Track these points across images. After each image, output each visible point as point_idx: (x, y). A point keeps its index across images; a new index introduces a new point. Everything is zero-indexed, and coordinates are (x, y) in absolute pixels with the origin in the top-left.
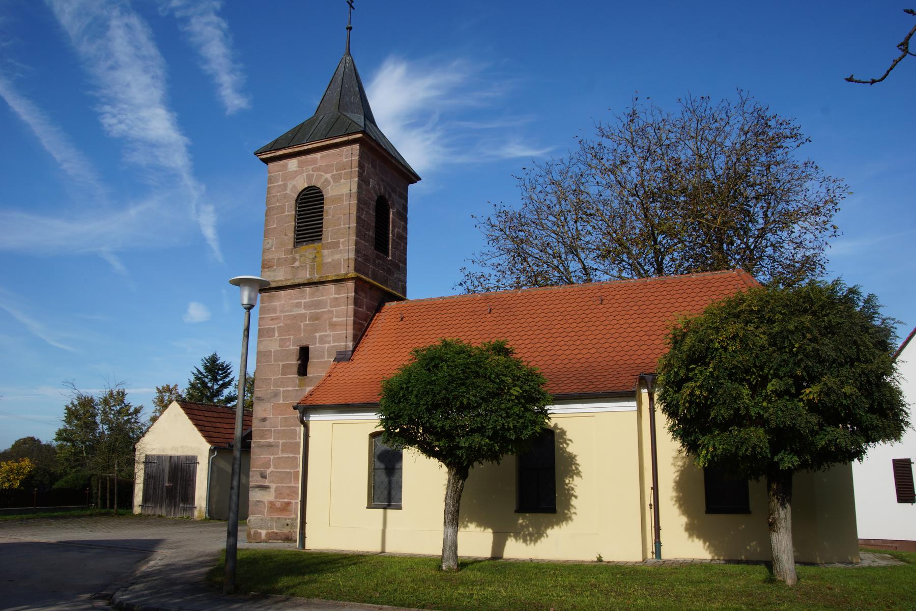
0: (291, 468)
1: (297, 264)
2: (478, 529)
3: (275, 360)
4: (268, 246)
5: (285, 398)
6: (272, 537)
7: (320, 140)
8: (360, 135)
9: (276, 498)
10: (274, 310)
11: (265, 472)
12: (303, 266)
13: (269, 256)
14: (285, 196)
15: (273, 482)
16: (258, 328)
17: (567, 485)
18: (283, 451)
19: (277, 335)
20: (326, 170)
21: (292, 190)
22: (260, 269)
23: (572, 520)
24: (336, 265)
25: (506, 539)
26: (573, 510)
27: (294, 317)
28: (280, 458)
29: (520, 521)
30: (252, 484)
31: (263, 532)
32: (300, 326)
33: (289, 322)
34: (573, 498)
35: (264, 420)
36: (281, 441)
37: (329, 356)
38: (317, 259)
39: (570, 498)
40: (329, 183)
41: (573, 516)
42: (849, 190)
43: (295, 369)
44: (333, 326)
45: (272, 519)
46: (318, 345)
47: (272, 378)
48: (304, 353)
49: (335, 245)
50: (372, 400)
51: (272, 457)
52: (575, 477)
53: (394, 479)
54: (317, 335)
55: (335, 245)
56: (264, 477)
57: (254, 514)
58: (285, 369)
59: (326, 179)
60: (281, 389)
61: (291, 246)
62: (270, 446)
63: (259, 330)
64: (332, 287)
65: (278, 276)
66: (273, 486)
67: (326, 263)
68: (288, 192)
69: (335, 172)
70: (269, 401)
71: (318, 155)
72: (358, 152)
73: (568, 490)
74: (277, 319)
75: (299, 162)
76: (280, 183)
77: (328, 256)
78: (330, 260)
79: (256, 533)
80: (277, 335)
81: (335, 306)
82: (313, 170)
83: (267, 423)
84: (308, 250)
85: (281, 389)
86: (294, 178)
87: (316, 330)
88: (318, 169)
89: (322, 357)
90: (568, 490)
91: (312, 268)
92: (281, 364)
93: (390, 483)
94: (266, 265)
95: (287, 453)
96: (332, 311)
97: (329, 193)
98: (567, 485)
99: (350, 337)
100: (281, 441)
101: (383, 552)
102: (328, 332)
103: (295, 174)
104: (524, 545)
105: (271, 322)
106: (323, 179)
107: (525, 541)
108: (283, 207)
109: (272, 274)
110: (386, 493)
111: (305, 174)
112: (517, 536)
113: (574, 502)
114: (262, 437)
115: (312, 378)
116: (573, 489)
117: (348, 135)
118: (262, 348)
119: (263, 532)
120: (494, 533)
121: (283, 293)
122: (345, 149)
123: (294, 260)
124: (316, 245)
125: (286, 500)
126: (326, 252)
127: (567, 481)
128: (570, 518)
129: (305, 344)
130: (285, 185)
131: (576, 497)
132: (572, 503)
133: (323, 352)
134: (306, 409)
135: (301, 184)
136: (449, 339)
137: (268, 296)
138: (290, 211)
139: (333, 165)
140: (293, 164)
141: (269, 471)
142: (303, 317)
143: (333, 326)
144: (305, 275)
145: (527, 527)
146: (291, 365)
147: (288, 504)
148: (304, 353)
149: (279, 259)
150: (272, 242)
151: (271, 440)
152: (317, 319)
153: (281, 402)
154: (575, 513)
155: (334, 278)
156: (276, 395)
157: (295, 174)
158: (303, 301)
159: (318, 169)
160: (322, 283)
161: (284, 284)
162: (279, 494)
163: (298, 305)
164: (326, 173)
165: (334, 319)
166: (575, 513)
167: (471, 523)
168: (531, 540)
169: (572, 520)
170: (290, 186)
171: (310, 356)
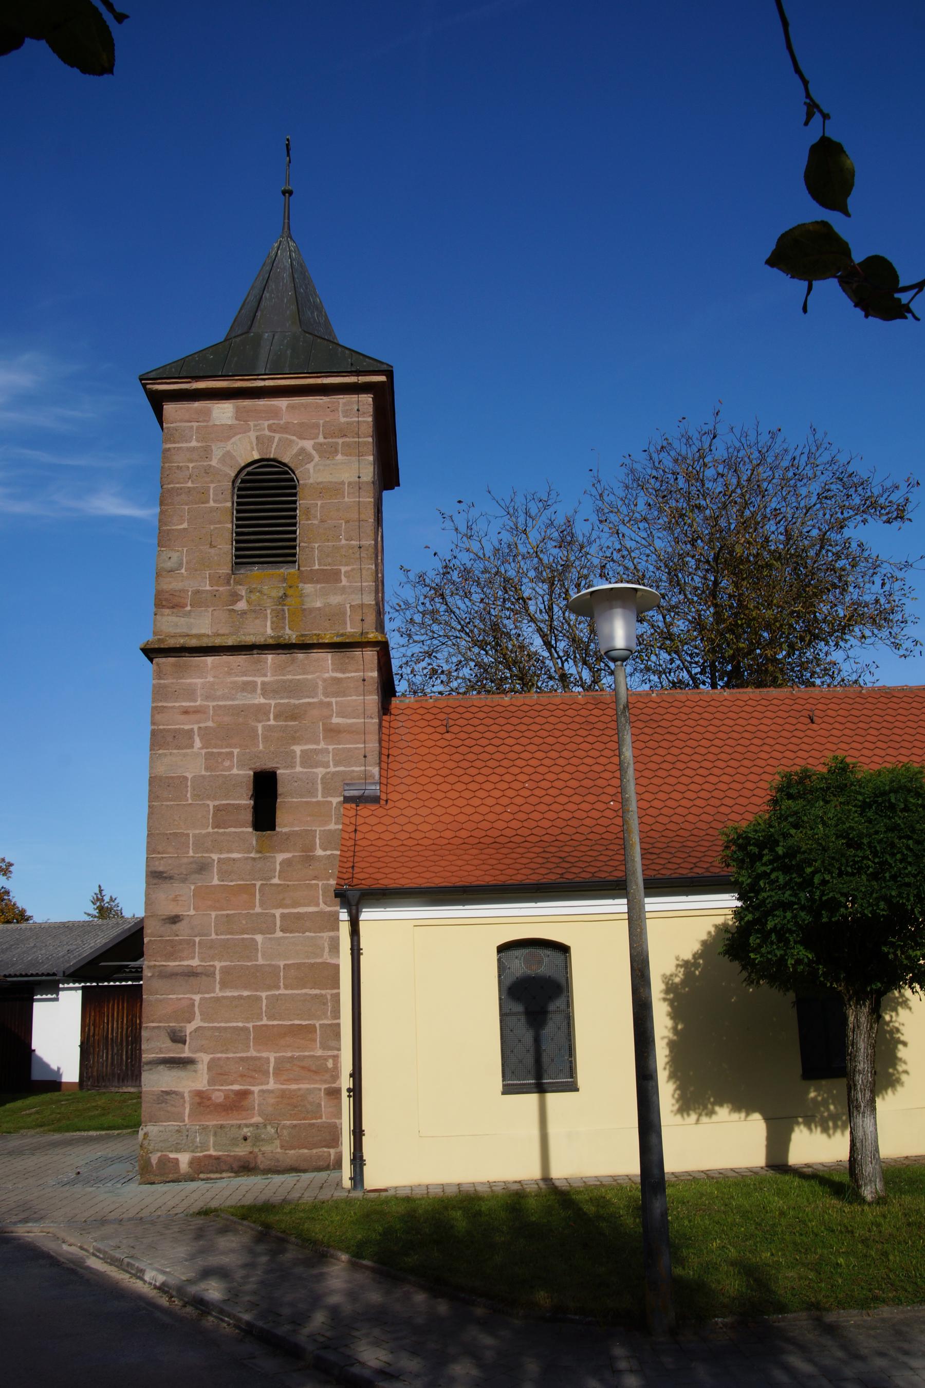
0: (247, 1020)
1: (242, 605)
2: (735, 1116)
3: (196, 796)
4: (169, 565)
5: (223, 875)
6: (205, 1168)
7: (296, 372)
8: (383, 378)
9: (211, 1082)
10: (190, 693)
11: (182, 1030)
12: (257, 611)
13: (171, 584)
14: (207, 471)
15: (202, 1049)
16: (149, 728)
17: (888, 1024)
18: (224, 985)
19: (198, 743)
20: (303, 431)
21: (222, 460)
22: (153, 609)
23: (902, 1084)
24: (336, 615)
25: (791, 1130)
26: (901, 1067)
27: (241, 710)
28: (217, 1000)
29: (812, 1095)
30: (146, 1057)
31: (184, 1159)
32: (255, 730)
33: (227, 719)
34: (900, 1047)
35: (175, 919)
36: (218, 965)
37: (327, 791)
38: (288, 601)
39: (896, 1047)
40: (310, 458)
41: (904, 1077)
42: (913, 595)
43: (248, 816)
44: (332, 732)
45: (205, 1128)
46: (299, 769)
47: (191, 832)
48: (265, 787)
49: (330, 577)
50: (718, 869)
51: (197, 998)
52: (900, 1009)
53: (549, 1030)
54: (298, 749)
55: (332, 577)
56: (178, 1038)
57: (154, 1120)
58: (222, 816)
59: (303, 450)
60: (215, 857)
61: (226, 570)
62: (192, 974)
63: (154, 733)
64: (327, 658)
65: (202, 625)
66: (204, 1059)
67: (311, 610)
68: (214, 463)
69: (321, 439)
70: (184, 880)
71: (282, 403)
72: (370, 409)
73: (891, 1032)
74: (197, 711)
75: (238, 410)
76: (194, 444)
77: (315, 597)
78: (319, 604)
79: (164, 1161)
80: (198, 743)
81: (336, 694)
82: (270, 428)
83: (180, 926)
84: (266, 581)
85: (215, 857)
86: (229, 438)
87: (295, 740)
88: (285, 428)
89: (312, 792)
90: (891, 1032)
91: (279, 616)
92: (211, 804)
93: (537, 1041)
94: (165, 601)
95: (236, 988)
96: (329, 704)
97: (313, 474)
98: (888, 1024)
99: (373, 757)
100: (282, 964)
101: (546, 1179)
102: (322, 745)
103: (228, 432)
104: (824, 1136)
105: (183, 718)
106: (295, 450)
107: (825, 1130)
108: (205, 492)
109: (183, 620)
110: (530, 1060)
111: (253, 435)
112: (809, 1121)
113: (902, 1052)
114: (171, 956)
115: (288, 836)
116: (898, 1030)
117: (358, 373)
118: (161, 770)
119: (184, 1159)
120: (767, 1119)
121: (209, 660)
122: (342, 400)
123: (235, 597)
124: (284, 570)
125: (236, 1087)
126: (308, 588)
127: (887, 1018)
128: (898, 1081)
129: (269, 765)
130: (206, 453)
131: (905, 1044)
132: (900, 1055)
133: (314, 783)
134: (355, 897)
135: (246, 451)
136: (849, 760)
137: (174, 665)
138: (221, 502)
139: (317, 426)
140: (223, 412)
141: (190, 1028)
142: (261, 712)
143: (332, 732)
144: (263, 629)
145: (825, 1103)
146: (238, 807)
147: (244, 1094)
148: (265, 787)
149: (197, 592)
150: (174, 556)
151: (195, 962)
152: (293, 718)
153: (216, 881)
154: (906, 1072)
155: (337, 640)
156: (203, 868)
157: (228, 432)
158: (259, 680)
159: (285, 428)
160: (305, 647)
161: (218, 642)
162: (218, 1072)
163: (249, 687)
164: (301, 438)
165: (335, 720)
166: (906, 1072)
167: (721, 1105)
168: (836, 1127)
169: (902, 1084)
170: (217, 452)
171: (280, 790)
